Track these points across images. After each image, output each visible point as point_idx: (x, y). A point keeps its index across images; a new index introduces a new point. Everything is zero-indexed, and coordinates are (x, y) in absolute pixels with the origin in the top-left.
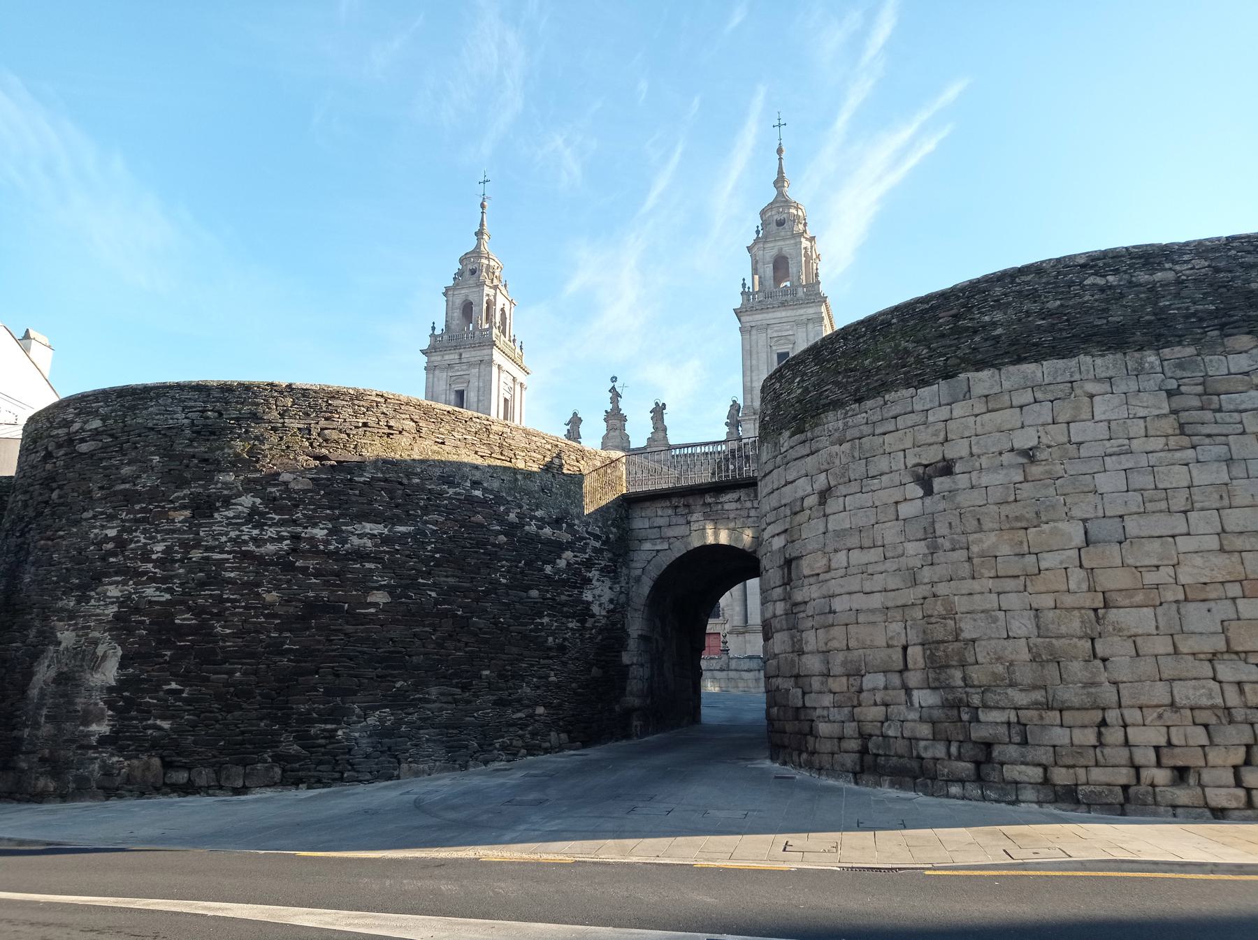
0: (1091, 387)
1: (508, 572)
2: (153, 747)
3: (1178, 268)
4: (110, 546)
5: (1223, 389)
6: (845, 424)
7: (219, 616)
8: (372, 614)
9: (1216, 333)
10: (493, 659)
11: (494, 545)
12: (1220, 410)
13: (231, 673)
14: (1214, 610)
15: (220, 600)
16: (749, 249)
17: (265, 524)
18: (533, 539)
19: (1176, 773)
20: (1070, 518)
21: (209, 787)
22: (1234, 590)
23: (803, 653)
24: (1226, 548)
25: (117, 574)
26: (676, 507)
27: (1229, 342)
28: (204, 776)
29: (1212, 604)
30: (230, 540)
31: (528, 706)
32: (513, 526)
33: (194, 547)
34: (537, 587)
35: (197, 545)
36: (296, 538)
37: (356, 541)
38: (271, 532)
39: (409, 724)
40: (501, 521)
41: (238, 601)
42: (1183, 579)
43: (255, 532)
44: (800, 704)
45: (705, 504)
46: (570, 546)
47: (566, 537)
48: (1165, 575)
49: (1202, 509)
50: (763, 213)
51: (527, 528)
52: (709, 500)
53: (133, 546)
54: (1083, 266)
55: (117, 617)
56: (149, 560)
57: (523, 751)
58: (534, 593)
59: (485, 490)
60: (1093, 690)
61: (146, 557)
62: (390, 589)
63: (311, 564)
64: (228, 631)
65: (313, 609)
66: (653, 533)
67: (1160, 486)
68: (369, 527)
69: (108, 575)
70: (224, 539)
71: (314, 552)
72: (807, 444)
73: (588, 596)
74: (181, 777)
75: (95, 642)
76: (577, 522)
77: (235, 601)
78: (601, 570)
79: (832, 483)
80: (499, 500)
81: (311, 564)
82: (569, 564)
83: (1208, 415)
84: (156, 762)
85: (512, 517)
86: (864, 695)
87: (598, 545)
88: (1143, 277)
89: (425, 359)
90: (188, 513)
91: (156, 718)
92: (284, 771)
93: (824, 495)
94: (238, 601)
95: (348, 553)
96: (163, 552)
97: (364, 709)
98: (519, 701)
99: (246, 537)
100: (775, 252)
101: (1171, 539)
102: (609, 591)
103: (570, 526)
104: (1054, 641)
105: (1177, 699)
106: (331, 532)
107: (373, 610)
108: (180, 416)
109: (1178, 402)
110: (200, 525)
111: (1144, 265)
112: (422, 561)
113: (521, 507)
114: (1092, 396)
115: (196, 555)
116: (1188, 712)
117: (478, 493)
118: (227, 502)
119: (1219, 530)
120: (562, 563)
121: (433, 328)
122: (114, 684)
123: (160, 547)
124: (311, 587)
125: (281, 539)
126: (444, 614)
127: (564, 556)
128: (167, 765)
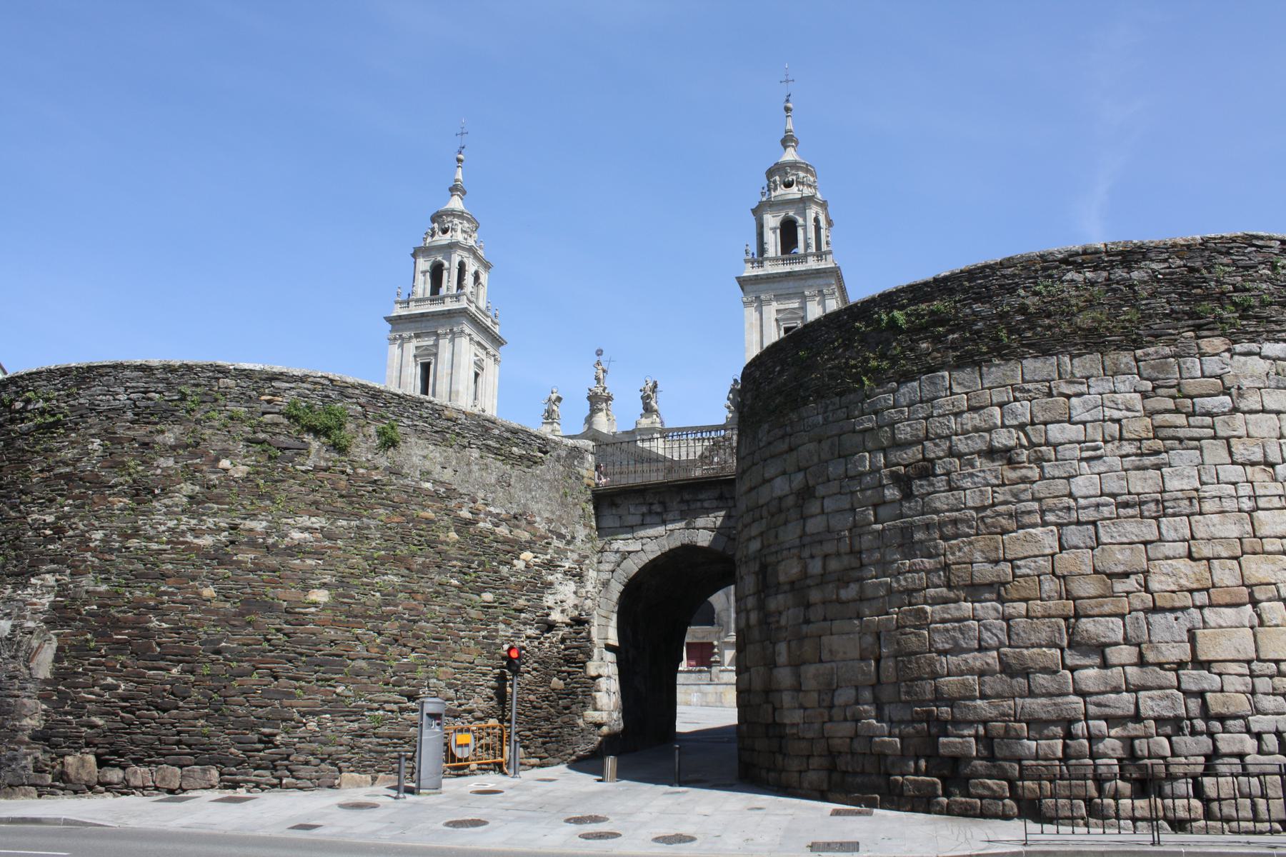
2: (87, 745)
5: (1195, 393)
6: (825, 419)
8: (312, 614)
9: (1192, 334)
10: (441, 666)
12: (1193, 414)
14: (1180, 620)
17: (204, 514)
19: (1137, 785)
20: (1045, 524)
21: (144, 788)
22: (1201, 598)
23: (776, 666)
24: (1195, 555)
25: (52, 561)
26: (651, 504)
27: (1204, 343)
28: (140, 774)
29: (1179, 614)
30: (169, 529)
36: (234, 527)
37: (297, 535)
38: (210, 522)
41: (175, 594)
42: (1154, 585)
43: (193, 522)
44: (770, 720)
45: (682, 501)
46: (529, 545)
47: (525, 536)
49: (1174, 515)
51: (481, 524)
52: (687, 497)
53: (71, 533)
54: (1065, 261)
55: (54, 606)
56: (88, 549)
58: (488, 597)
59: (435, 482)
60: (1059, 700)
61: (84, 542)
64: (165, 625)
67: (1133, 491)
68: (305, 521)
69: (43, 562)
70: (162, 528)
71: (252, 544)
72: (787, 440)
74: (115, 775)
76: (538, 519)
77: (173, 594)
78: (565, 573)
79: (811, 483)
80: (451, 493)
82: (527, 566)
83: (1180, 419)
85: (465, 514)
86: (834, 711)
92: (221, 774)
93: (806, 493)
94: (175, 594)
95: (288, 548)
96: (101, 541)
98: (470, 712)
99: (184, 527)
101: (1142, 546)
102: (573, 596)
103: (530, 523)
104: (1025, 652)
105: (1142, 711)
107: (313, 610)
108: (123, 397)
109: (1153, 403)
111: (1122, 263)
115: (133, 543)
117: (428, 485)
119: (1188, 536)
120: (520, 565)
122: (49, 676)
123: (99, 535)
127: (522, 556)
128: (101, 763)
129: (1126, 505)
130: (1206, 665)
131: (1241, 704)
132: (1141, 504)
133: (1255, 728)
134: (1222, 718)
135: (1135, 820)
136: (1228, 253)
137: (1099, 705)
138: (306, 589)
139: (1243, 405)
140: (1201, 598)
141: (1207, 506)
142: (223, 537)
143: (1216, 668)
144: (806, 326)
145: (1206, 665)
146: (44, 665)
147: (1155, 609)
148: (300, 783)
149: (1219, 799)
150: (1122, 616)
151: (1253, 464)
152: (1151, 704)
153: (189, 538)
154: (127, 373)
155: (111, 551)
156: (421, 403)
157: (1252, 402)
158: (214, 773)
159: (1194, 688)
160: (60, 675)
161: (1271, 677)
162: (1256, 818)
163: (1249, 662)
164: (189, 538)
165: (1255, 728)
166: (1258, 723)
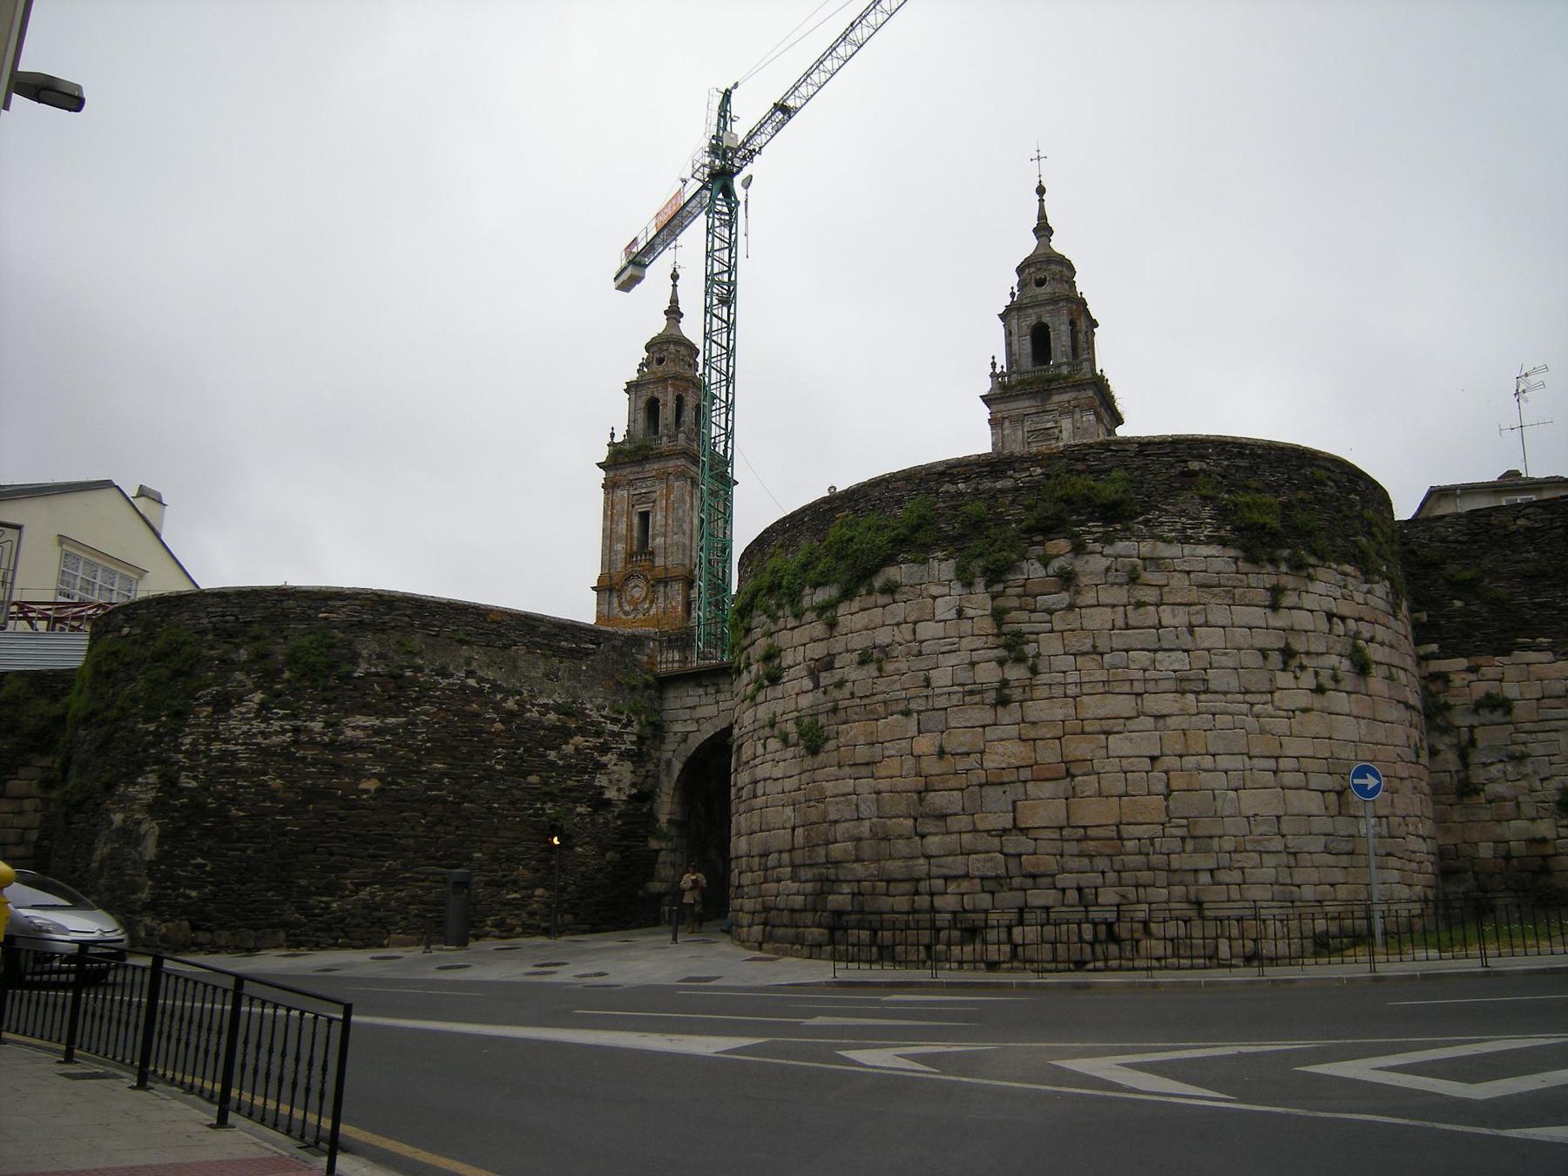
0: (934, 590)
1: (504, 758)
3: (1017, 475)
4: (150, 738)
7: (233, 800)
11: (489, 733)
12: (1034, 611)
13: (243, 850)
15: (235, 786)
16: (1003, 317)
18: (536, 725)
22: (1025, 774)
28: (224, 936)
29: (1006, 787)
31: (526, 888)
32: (511, 713)
33: (214, 740)
34: (538, 773)
35: (217, 738)
37: (349, 733)
38: (276, 725)
39: (399, 899)
40: (497, 708)
48: (971, 761)
50: (1020, 270)
54: (942, 474)
55: (156, 799)
57: (519, 930)
58: (534, 779)
59: (481, 680)
62: (379, 777)
63: (309, 754)
65: (311, 794)
66: (687, 714)
68: (361, 720)
70: (238, 732)
73: (601, 780)
74: (203, 937)
75: (139, 823)
81: (309, 754)
82: (577, 749)
83: (1024, 616)
84: (186, 924)
85: (510, 704)
87: (616, 728)
88: (987, 484)
89: (602, 473)
90: (210, 709)
91: (186, 887)
97: (356, 885)
98: (515, 882)
100: (1033, 320)
102: (630, 776)
104: (889, 822)
106: (328, 725)
110: (219, 720)
112: (413, 751)
113: (520, 694)
114: (934, 598)
115: (216, 746)
116: (978, 881)
117: (472, 682)
118: (240, 700)
120: (569, 749)
121: (612, 435)
124: (308, 775)
125: (284, 732)
126: (435, 799)
128: (195, 928)
129: (972, 693)
130: (1024, 831)
131: (1051, 863)
132: (980, 692)
133: (1059, 885)
134: (1034, 876)
135: (961, 962)
136: (1084, 460)
137: (939, 866)
138: (358, 780)
139: (1081, 601)
140: (1025, 774)
141: (1038, 693)
142: (288, 737)
143: (1032, 834)
144: (1105, 446)
145: (1024, 831)
146: (150, 850)
147: (988, 784)
148: (355, 943)
149: (1024, 945)
150: (961, 790)
151: (1084, 654)
152: (976, 864)
153: (259, 739)
154: (209, 600)
155: (199, 752)
156: (1109, 443)
157: (1088, 597)
158: (282, 935)
159: (1012, 851)
160: (161, 857)
161: (1078, 841)
162: (1054, 960)
163: (1061, 828)
164: (259, 739)
165: (1059, 885)
166: (1065, 880)
